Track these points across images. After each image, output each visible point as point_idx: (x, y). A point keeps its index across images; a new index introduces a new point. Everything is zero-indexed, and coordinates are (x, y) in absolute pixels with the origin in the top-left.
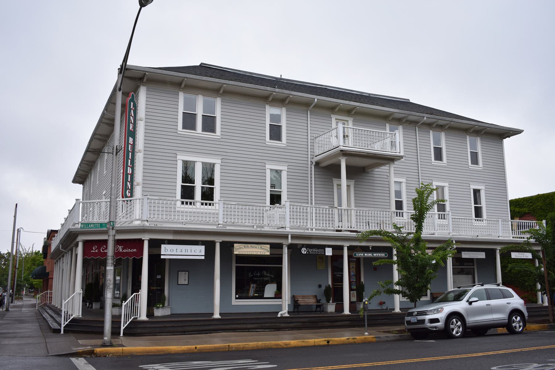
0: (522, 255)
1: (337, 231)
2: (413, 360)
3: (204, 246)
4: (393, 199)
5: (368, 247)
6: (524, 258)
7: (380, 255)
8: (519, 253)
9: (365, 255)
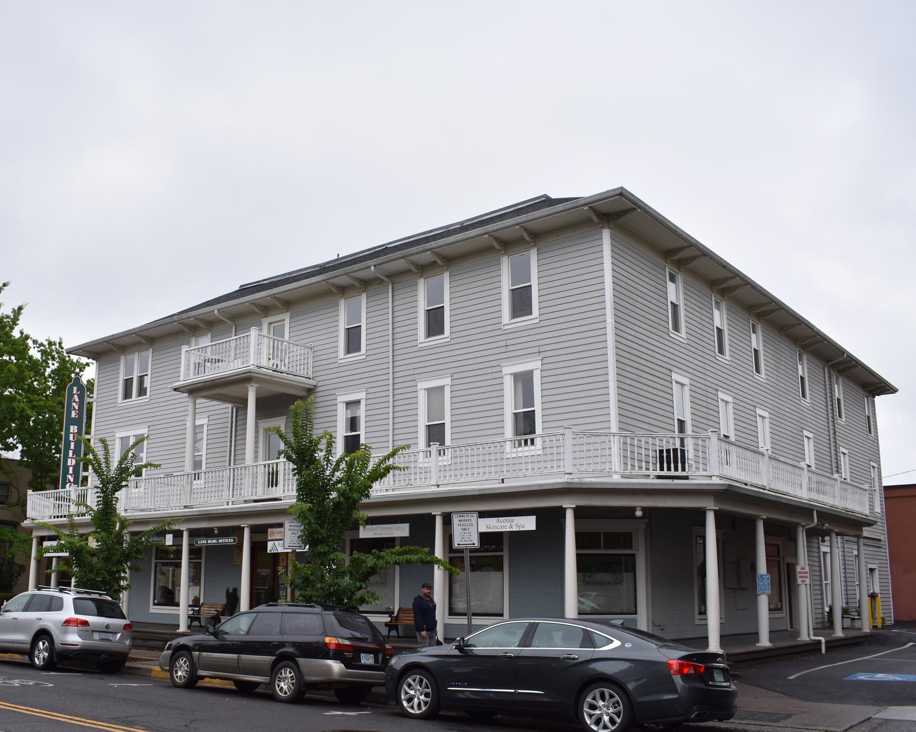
0: (505, 524)
1: (185, 507)
2: (92, 724)
3: (535, 516)
4: (510, 408)
5: (212, 529)
6: (511, 530)
7: (227, 541)
8: (499, 518)
9: (209, 542)
